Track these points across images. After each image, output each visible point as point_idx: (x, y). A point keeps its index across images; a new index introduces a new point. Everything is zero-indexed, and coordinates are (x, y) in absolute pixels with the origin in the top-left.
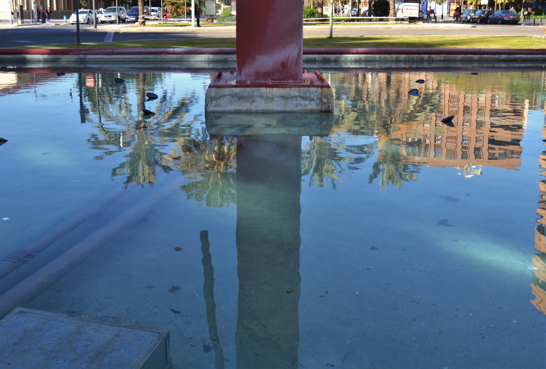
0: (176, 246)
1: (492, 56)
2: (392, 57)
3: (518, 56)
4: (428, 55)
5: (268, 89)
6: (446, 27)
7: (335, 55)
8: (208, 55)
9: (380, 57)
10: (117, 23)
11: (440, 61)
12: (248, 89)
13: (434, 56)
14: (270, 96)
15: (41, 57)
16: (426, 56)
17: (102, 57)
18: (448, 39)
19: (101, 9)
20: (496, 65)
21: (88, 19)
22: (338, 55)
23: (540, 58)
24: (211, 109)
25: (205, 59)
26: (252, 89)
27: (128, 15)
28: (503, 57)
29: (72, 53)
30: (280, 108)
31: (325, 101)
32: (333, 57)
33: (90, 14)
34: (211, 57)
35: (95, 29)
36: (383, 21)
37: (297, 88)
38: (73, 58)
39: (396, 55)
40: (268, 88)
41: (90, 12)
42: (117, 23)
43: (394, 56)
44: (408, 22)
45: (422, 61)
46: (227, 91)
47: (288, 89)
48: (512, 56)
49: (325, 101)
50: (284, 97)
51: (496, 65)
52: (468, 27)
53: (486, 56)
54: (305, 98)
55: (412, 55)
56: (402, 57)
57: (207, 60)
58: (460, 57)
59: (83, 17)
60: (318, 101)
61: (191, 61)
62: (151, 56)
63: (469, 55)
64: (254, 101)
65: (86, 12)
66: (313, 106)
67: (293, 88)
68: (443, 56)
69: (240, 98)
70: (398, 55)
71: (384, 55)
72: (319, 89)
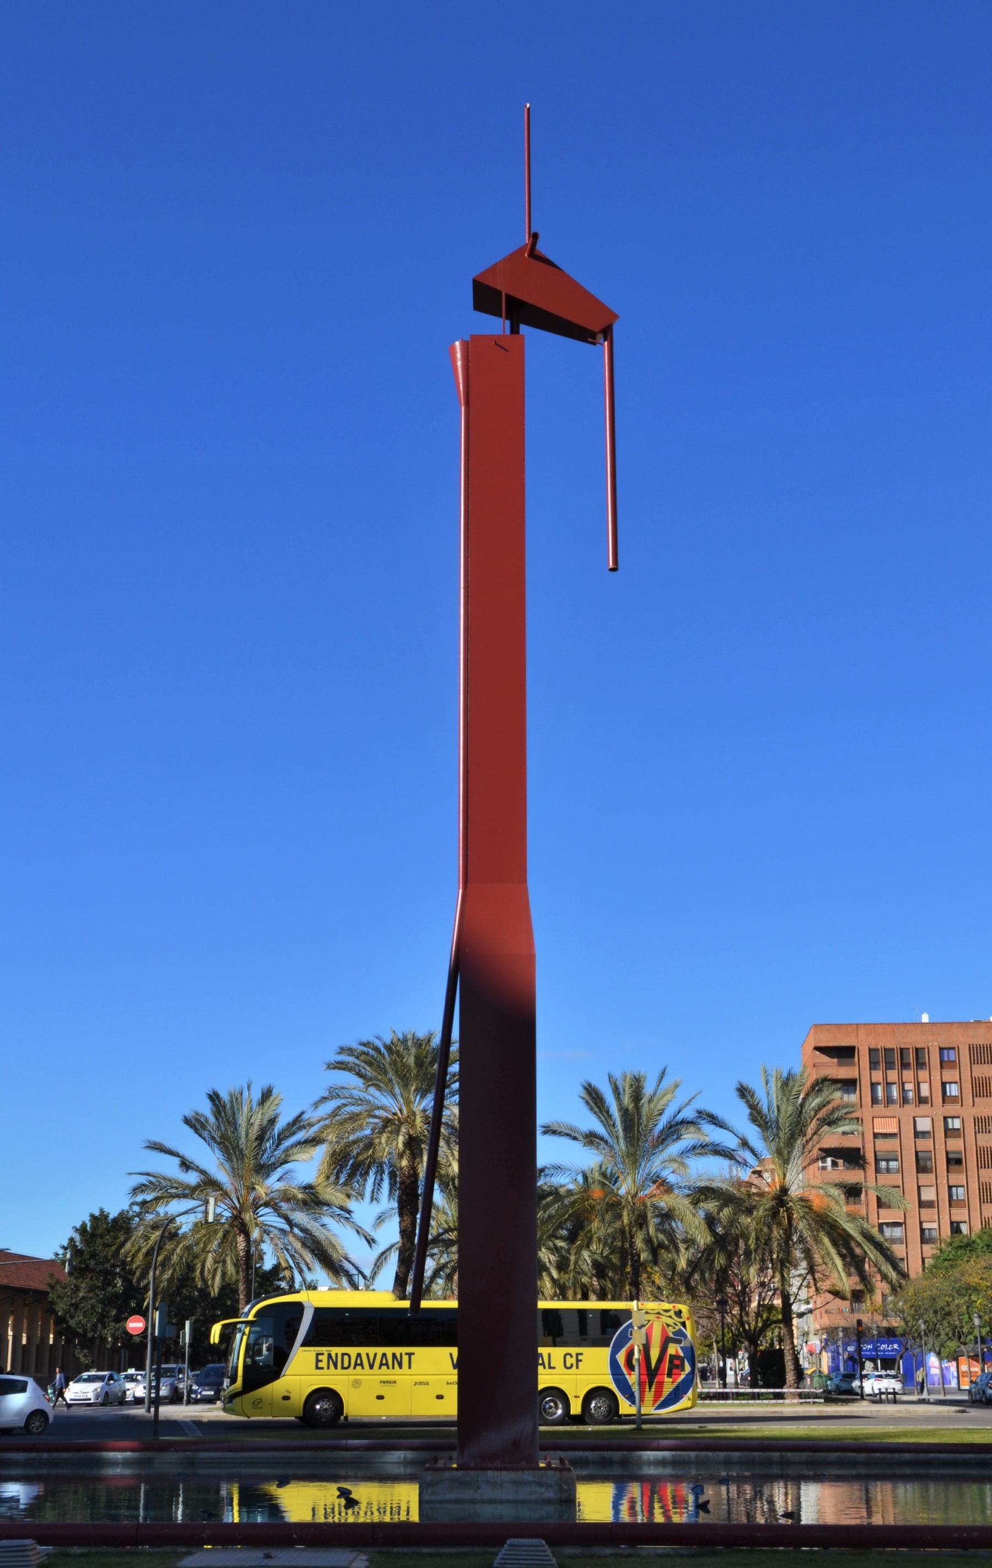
0: (617, 572)
1: (889, 1455)
2: (717, 1456)
3: (932, 1455)
4: (779, 1454)
5: (496, 1473)
6: (900, 1411)
7: (620, 1453)
8: (404, 1452)
9: (697, 1456)
10: (185, 1402)
11: (800, 1463)
12: (472, 1473)
13: (789, 1454)
14: (499, 1481)
15: (119, 1457)
16: (776, 1455)
17: (10, 1545)
18: (866, 1431)
19: (131, 1371)
20: (897, 1471)
21: (107, 1393)
22: (626, 1453)
23: (970, 1459)
24: (427, 1497)
25: (400, 1458)
26: (476, 1472)
27: (199, 1385)
28: (907, 1456)
29: (173, 1449)
30: (511, 1497)
31: (566, 1487)
32: (617, 1455)
33: (112, 1382)
34: (410, 1455)
35: (147, 1414)
36: (759, 1399)
37: (532, 1472)
38: (174, 1457)
39: (725, 1453)
40: (496, 1472)
41: (111, 1378)
42: (185, 1402)
43: (722, 1454)
44: (822, 1400)
45: (769, 1463)
46: (446, 1474)
47: (520, 1472)
48: (922, 1456)
49: (566, 1487)
50: (516, 1483)
51: (897, 1471)
52: (948, 1412)
53: (878, 1455)
54: (541, 1484)
55: (753, 1453)
56: (736, 1455)
57: (402, 1460)
58: (833, 1456)
59: (96, 1390)
60: (556, 1488)
61: (373, 1463)
62: (306, 1454)
63: (849, 1454)
64: (478, 1488)
65: (101, 1379)
66: (550, 1494)
67: (525, 1472)
68: (805, 1454)
69: (463, 1483)
70: (729, 1453)
71: (703, 1453)
72: (558, 1473)
